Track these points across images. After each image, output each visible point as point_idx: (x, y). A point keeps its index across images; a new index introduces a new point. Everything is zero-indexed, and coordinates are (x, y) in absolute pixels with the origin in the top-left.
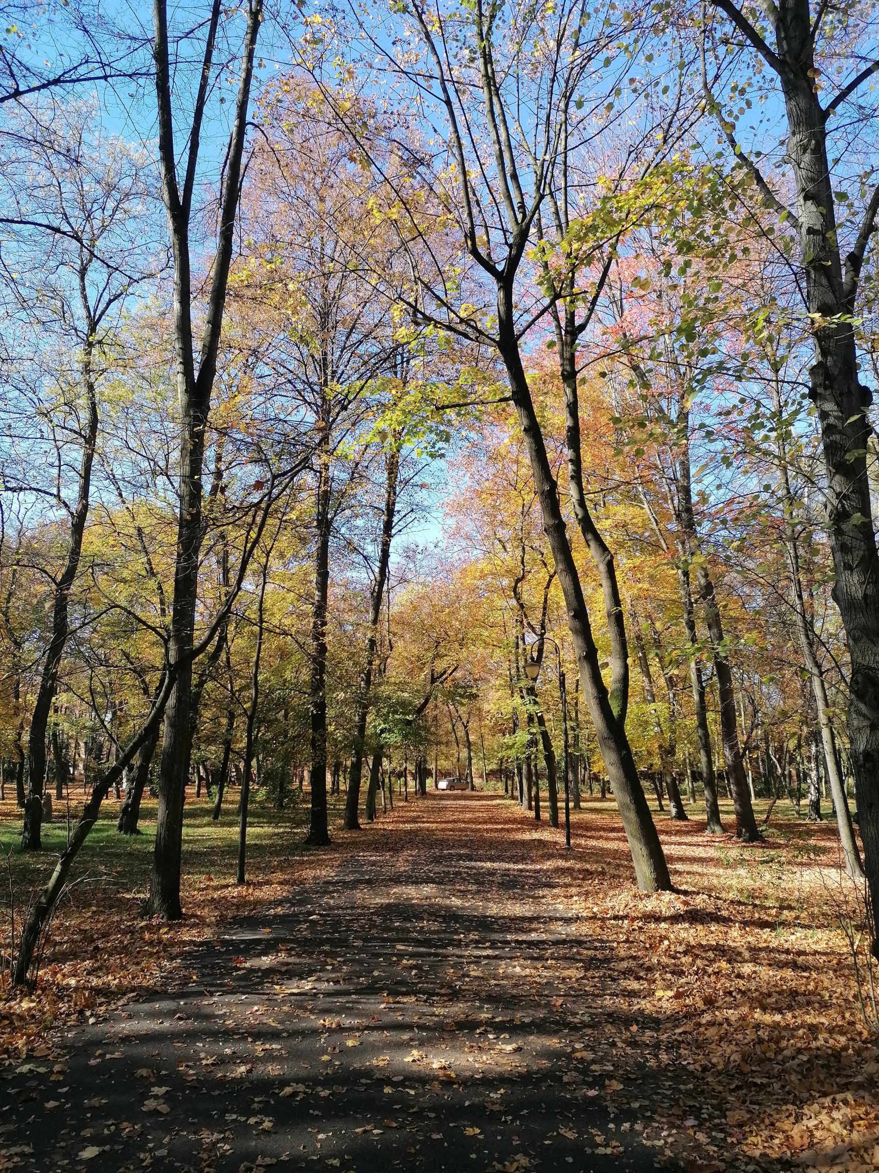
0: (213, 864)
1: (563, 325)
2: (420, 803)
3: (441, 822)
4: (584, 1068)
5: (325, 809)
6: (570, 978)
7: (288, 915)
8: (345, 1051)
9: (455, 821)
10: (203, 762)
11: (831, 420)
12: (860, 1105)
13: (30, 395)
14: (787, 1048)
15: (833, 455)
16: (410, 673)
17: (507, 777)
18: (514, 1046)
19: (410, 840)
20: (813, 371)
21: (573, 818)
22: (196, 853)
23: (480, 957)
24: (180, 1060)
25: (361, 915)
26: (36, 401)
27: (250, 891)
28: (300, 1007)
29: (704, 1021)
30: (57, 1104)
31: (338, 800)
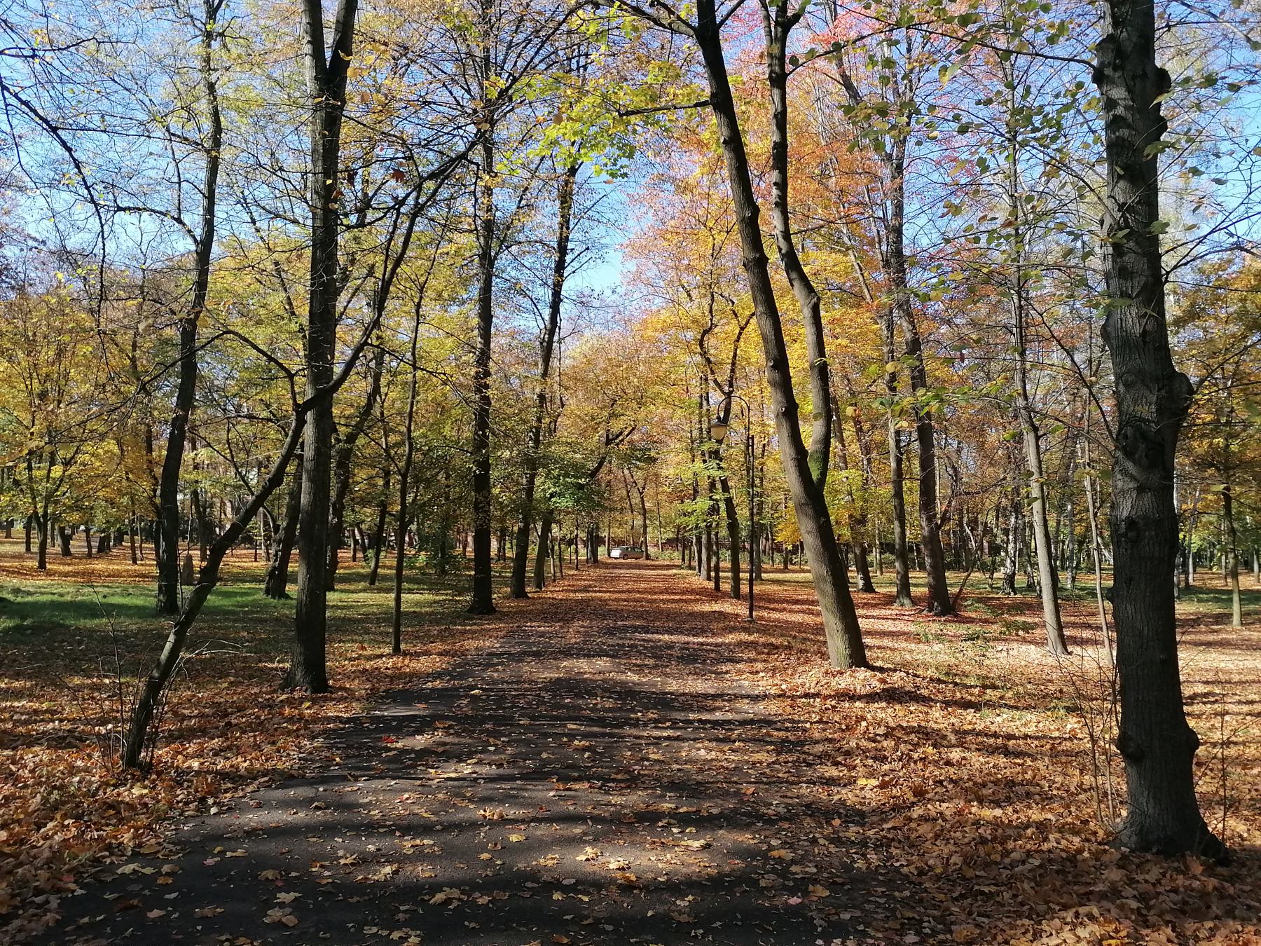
0: (367, 632)
1: (773, 15)
2: (591, 571)
3: (614, 592)
4: (782, 869)
5: (489, 576)
6: (761, 763)
7: (446, 689)
8: (508, 848)
9: (628, 591)
10: (358, 525)
11: (1120, 111)
12: (1110, 922)
13: (140, 96)
14: (1014, 850)
15: (1119, 155)
16: (583, 433)
17: (685, 548)
18: (702, 842)
19: (583, 609)
20: (1100, 47)
21: (757, 589)
22: (349, 620)
23: (660, 738)
24: (315, 858)
25: (529, 690)
26: (147, 102)
27: (407, 662)
28: (457, 795)
29: (915, 816)
30: (162, 913)
31: (504, 568)
